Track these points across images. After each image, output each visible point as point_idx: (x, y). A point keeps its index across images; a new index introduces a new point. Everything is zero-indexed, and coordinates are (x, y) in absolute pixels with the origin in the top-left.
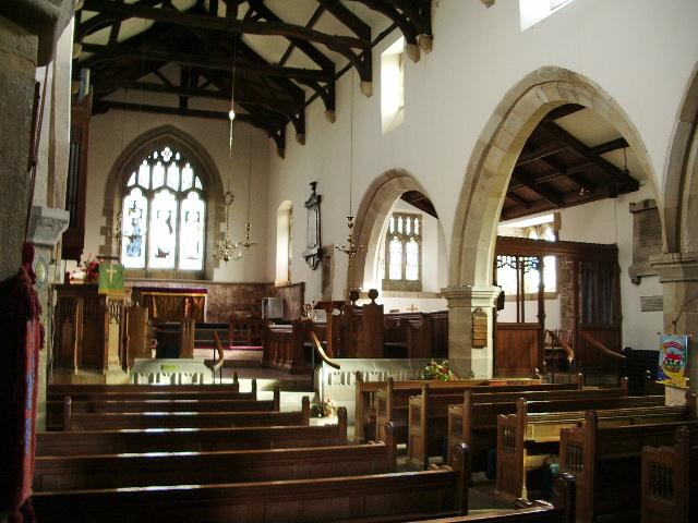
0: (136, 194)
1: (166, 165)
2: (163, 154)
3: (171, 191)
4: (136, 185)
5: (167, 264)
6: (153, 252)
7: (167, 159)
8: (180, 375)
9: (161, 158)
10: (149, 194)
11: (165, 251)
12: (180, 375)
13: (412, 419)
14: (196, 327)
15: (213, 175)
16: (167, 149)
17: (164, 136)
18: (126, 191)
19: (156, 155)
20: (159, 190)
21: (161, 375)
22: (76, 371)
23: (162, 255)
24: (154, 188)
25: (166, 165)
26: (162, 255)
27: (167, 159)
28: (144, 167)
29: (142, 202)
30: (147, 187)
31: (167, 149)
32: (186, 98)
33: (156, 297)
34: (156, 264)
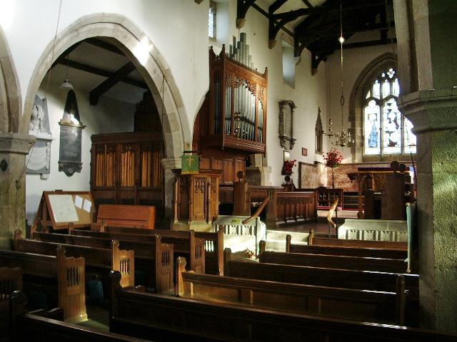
0: (372, 103)
1: (391, 81)
2: (388, 73)
3: (376, 100)
4: (372, 98)
5: (396, 150)
6: (386, 143)
7: (391, 76)
8: (379, 232)
9: (387, 76)
10: (380, 103)
11: (394, 141)
12: (379, 232)
13: (61, 319)
14: (291, 191)
15: (54, 47)
16: (391, 70)
17: (385, 61)
18: (364, 103)
19: (383, 75)
20: (387, 99)
21: (231, 226)
22: (176, 221)
23: (392, 144)
24: (384, 97)
25: (391, 81)
26: (392, 144)
27: (391, 76)
28: (376, 86)
29: (377, 108)
30: (379, 98)
31: (391, 70)
32: (386, 31)
33: (374, 174)
34: (388, 151)
